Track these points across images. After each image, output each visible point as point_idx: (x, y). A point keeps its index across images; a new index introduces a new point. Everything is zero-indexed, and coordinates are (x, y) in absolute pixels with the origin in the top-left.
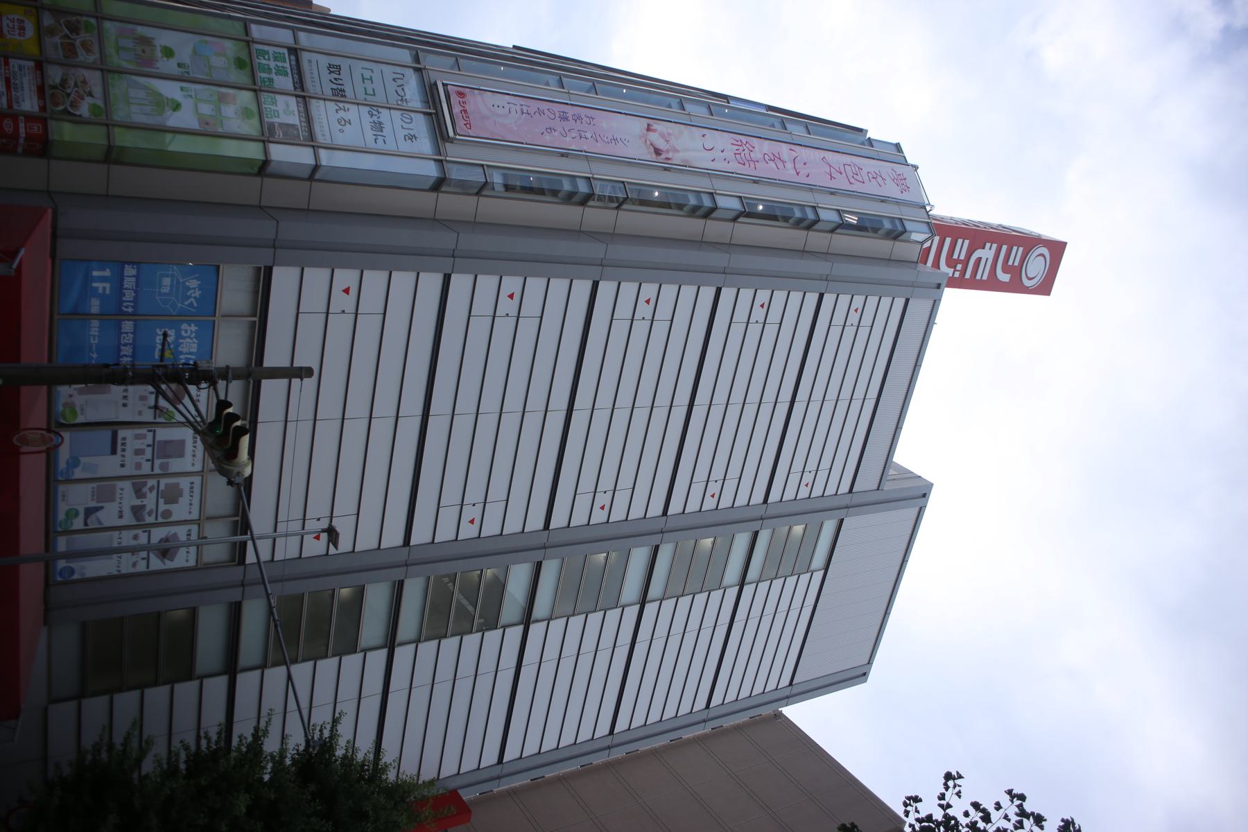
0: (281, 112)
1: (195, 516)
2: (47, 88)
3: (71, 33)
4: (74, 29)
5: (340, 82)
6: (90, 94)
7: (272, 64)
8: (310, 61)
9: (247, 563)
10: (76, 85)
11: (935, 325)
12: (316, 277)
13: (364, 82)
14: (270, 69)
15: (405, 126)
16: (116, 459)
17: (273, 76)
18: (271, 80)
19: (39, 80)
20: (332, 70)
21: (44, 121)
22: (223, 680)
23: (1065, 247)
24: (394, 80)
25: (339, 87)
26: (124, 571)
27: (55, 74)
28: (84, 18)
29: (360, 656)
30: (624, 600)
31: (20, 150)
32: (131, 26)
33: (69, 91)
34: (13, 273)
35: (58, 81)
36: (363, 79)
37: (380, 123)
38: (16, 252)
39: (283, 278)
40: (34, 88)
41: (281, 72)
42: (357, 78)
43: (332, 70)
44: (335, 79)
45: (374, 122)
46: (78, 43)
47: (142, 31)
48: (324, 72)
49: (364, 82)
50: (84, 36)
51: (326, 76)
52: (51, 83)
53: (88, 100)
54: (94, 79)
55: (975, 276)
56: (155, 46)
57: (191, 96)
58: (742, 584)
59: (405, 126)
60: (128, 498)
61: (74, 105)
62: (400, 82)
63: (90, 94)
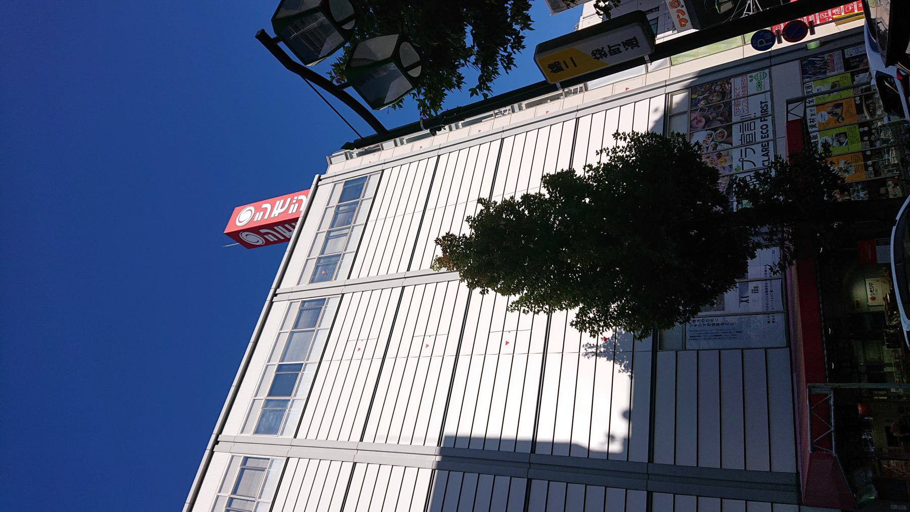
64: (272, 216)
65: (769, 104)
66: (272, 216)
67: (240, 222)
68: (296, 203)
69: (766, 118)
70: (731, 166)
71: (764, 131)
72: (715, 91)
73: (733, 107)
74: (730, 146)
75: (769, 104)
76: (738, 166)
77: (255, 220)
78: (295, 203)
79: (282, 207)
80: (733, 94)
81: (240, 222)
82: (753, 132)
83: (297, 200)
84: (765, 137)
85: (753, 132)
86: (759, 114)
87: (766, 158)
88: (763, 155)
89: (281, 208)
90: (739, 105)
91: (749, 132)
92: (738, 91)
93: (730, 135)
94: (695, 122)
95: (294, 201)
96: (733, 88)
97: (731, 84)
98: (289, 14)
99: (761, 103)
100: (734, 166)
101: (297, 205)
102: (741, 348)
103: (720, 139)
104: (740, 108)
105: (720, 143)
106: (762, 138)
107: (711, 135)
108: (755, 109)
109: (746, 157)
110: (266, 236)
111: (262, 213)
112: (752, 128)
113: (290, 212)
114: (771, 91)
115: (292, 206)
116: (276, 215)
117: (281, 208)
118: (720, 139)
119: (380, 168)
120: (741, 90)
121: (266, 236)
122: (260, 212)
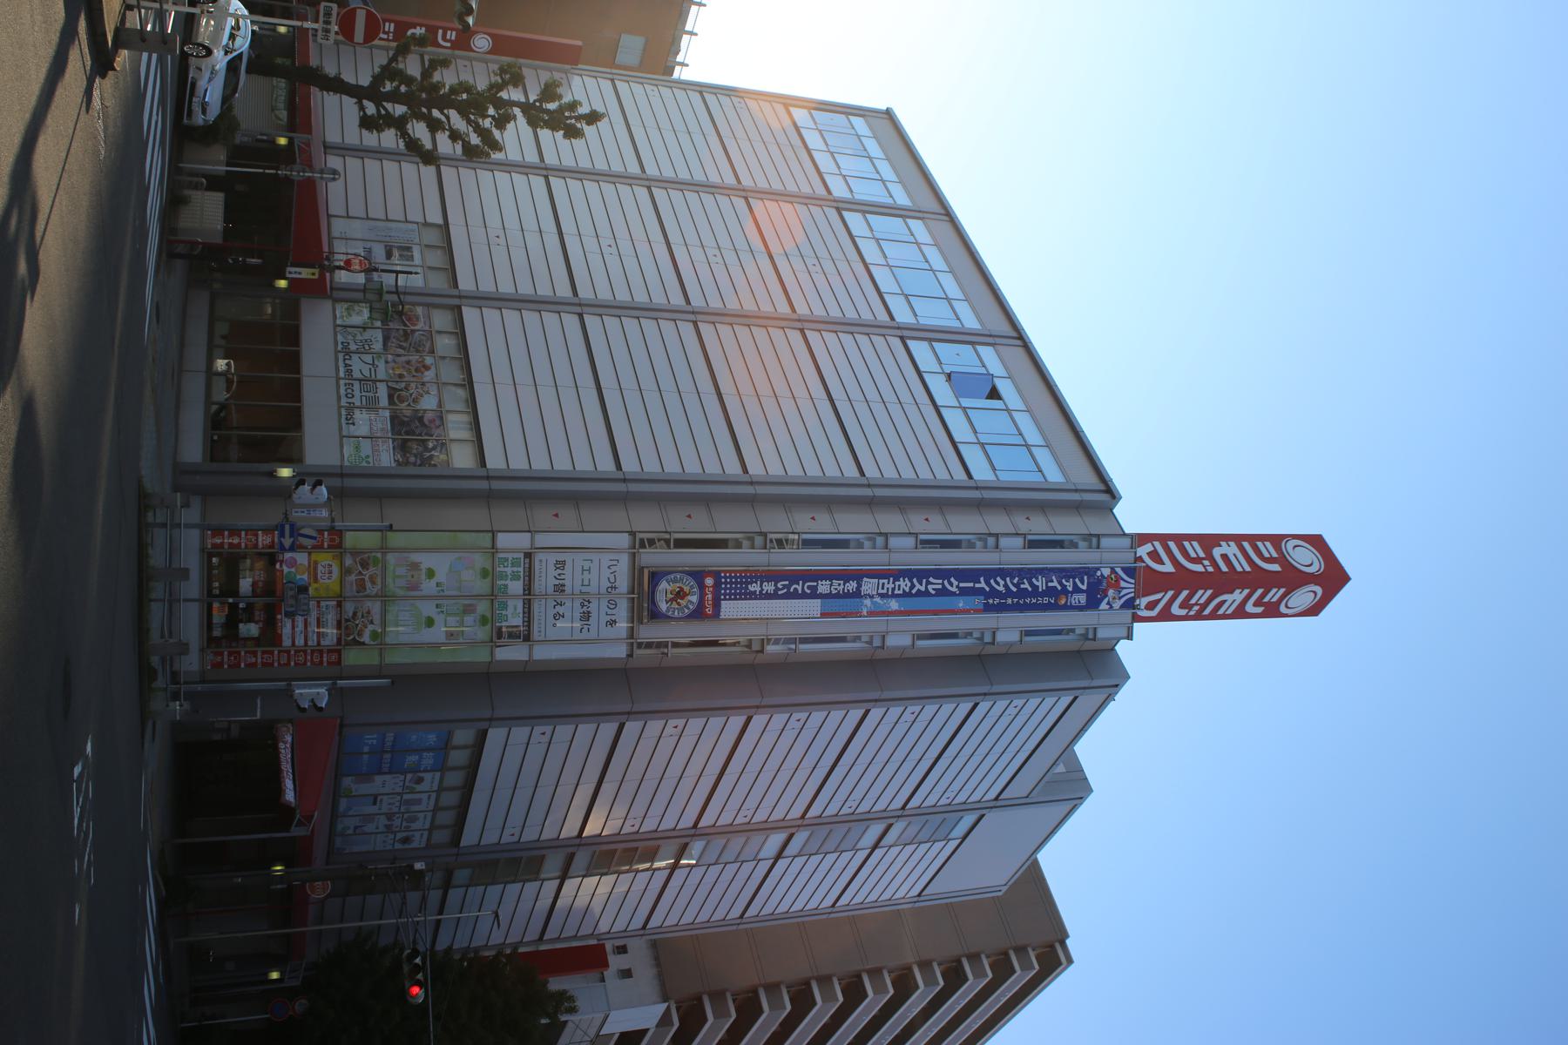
0: (510, 616)
1: (435, 788)
2: (343, 622)
3: (363, 569)
4: (365, 565)
5: (563, 577)
6: (372, 622)
7: (509, 570)
8: (541, 561)
9: (462, 845)
10: (363, 616)
11: (1113, 702)
12: (520, 733)
13: (582, 573)
14: (507, 576)
15: (610, 612)
16: (377, 807)
17: (508, 582)
18: (506, 586)
19: (339, 616)
20: (558, 566)
21: (339, 652)
22: (440, 892)
23: (1346, 583)
24: (609, 567)
25: (561, 582)
26: (377, 849)
27: (349, 608)
28: (373, 554)
29: (539, 883)
30: (761, 856)
31: (326, 545)
32: (406, 555)
33: (357, 622)
34: (309, 833)
35: (351, 614)
36: (583, 570)
37: (589, 612)
38: (312, 816)
39: (495, 736)
40: (335, 623)
41: (515, 577)
42: (578, 570)
43: (558, 566)
44: (559, 575)
45: (584, 612)
46: (367, 578)
47: (415, 557)
48: (551, 567)
49: (582, 573)
50: (372, 570)
51: (552, 572)
52: (346, 617)
53: (370, 627)
54: (375, 607)
55: (1217, 611)
56: (421, 570)
57: (442, 612)
58: (876, 846)
59: (610, 612)
60: (383, 820)
61: (360, 634)
62: (613, 569)
63: (372, 622)
64: (1246, 591)
65: (343, 421)
66: (1246, 591)
67: (1315, 593)
68: (1194, 605)
69: (348, 405)
70: (387, 362)
71: (349, 391)
72: (416, 456)
73: (389, 428)
74: (390, 384)
75: (343, 421)
76: (378, 360)
77: (1282, 591)
78: (1196, 604)
79: (1222, 603)
80: (391, 446)
81: (1315, 593)
82: (364, 394)
83: (1190, 609)
84: (349, 384)
85: (364, 394)
86: (357, 412)
87: (347, 362)
88: (350, 366)
89: (1226, 601)
90: (382, 429)
91: (367, 394)
92: (385, 447)
93: (390, 397)
94: (438, 423)
95: (1196, 608)
96: (392, 455)
97: (395, 461)
98: (44, 76)
99: (354, 424)
100: (383, 361)
101: (1193, 601)
102: (369, 221)
103: (404, 393)
104: (380, 426)
105: (401, 390)
106: (352, 385)
107: (413, 401)
108: (361, 417)
109: (370, 369)
110: (1275, 555)
111: (1266, 600)
112: (364, 398)
113: (1209, 592)
114: (342, 437)
115: (1202, 601)
116: (1238, 591)
117: (1226, 601)
118: (404, 393)
119: (999, 803)
120: (381, 449)
121: (1275, 555)
122: (1269, 602)
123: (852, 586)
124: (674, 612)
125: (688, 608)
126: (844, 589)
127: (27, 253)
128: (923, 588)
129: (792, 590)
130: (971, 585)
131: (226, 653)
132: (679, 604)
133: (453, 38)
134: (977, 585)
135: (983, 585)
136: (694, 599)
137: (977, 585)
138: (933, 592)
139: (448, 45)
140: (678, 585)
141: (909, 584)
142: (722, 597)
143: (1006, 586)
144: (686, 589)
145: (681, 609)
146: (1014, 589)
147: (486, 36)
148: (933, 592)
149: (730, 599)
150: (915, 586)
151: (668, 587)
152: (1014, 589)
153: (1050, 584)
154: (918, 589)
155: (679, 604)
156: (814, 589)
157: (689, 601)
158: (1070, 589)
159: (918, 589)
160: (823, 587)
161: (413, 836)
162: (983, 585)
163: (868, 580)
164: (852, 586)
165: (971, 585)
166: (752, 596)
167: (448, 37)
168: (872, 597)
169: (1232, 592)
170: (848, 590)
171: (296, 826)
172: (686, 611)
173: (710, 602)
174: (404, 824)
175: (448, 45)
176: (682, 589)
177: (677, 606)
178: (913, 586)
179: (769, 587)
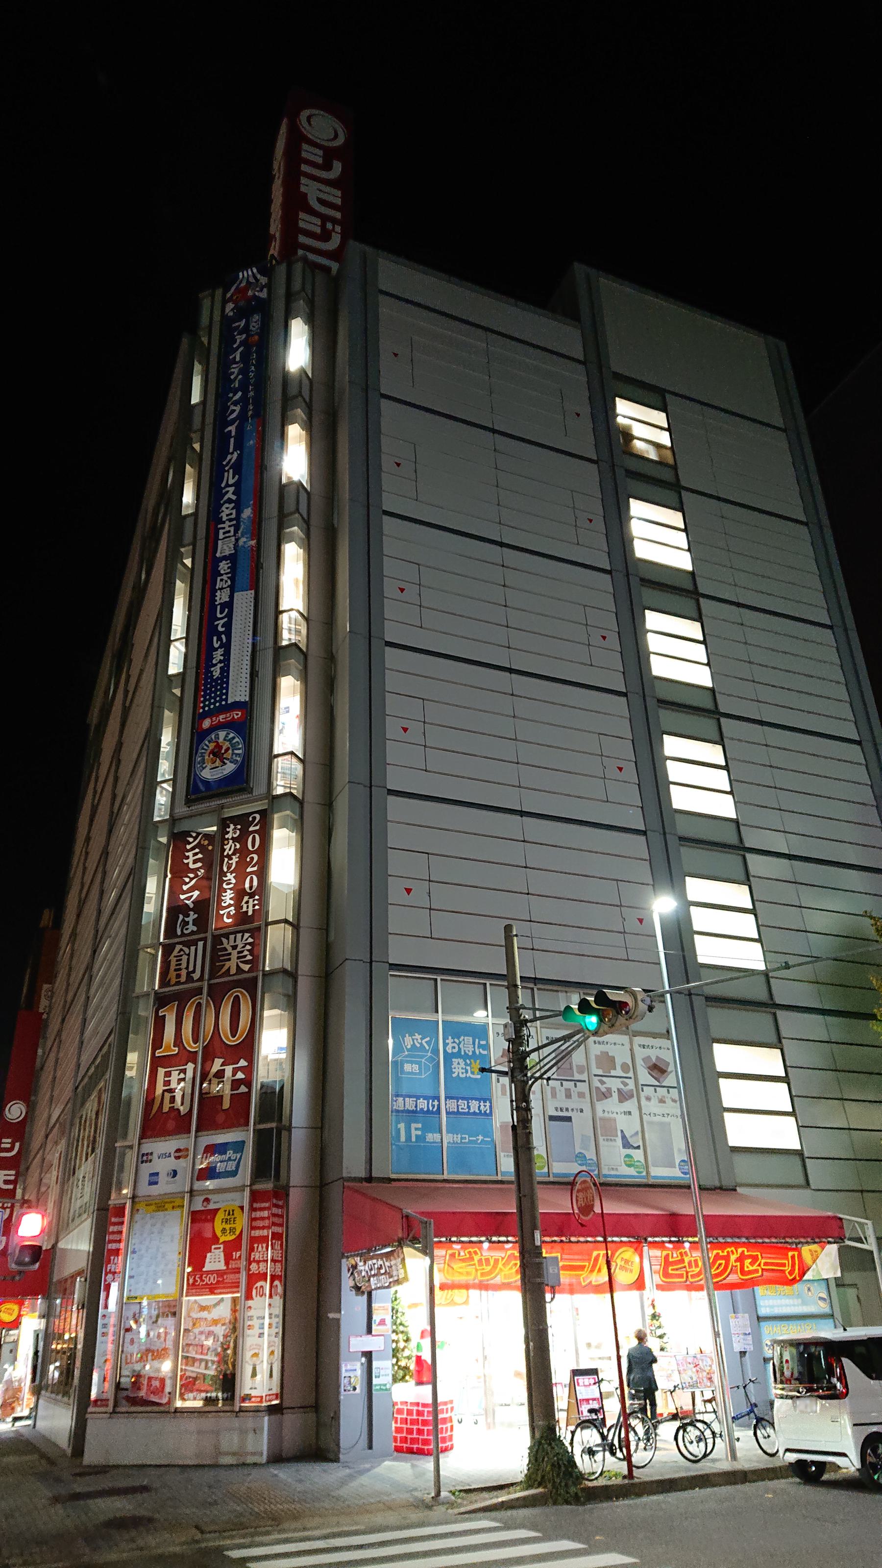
67: (336, 136)
79: (321, 201)
81: (336, 136)
123: (224, 566)
124: (237, 754)
125: (233, 738)
126: (226, 574)
127: (579, 1550)
128: (232, 489)
129: (223, 629)
130: (232, 440)
131: (238, 1295)
132: (227, 750)
133: (9, 1140)
134: (233, 434)
135: (232, 429)
136: (222, 734)
137: (233, 434)
138: (237, 477)
139: (17, 1145)
140: (206, 757)
141: (227, 505)
142: (224, 703)
143: (235, 403)
144: (212, 746)
145: (234, 747)
146: (240, 394)
147: (23, 1116)
148: (237, 477)
149: (227, 694)
150: (229, 499)
151: (209, 767)
152: (240, 394)
153: (238, 359)
154: (233, 493)
155: (227, 750)
156: (224, 605)
157: (225, 740)
158: (244, 336)
159: (233, 493)
160: (222, 597)
161: (646, 1059)
162: (232, 429)
163: (219, 551)
164: (224, 566)
165: (232, 440)
166: (225, 671)
167: (9, 1146)
168: (237, 540)
169: (305, 195)
170: (228, 568)
171: (810, 1250)
172: (237, 740)
173: (228, 715)
174: (618, 1072)
175: (17, 1145)
176: (212, 752)
177: (230, 751)
178: (229, 501)
179: (218, 655)
